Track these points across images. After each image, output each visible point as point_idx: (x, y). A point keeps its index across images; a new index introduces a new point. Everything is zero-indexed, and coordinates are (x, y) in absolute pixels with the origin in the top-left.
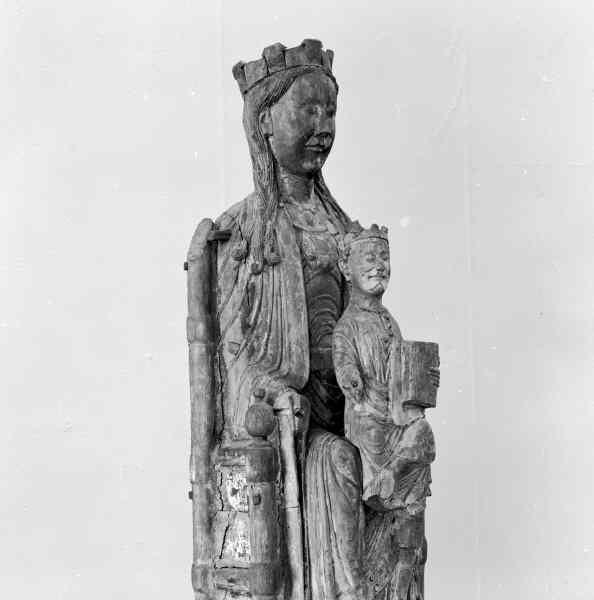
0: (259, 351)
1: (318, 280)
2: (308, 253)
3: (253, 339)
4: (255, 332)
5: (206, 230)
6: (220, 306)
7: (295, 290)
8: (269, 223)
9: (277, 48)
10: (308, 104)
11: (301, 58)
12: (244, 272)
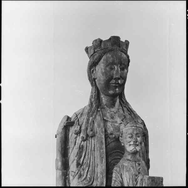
0: (84, 176)
1: (113, 144)
2: (109, 132)
3: (81, 170)
4: (82, 167)
5: (65, 120)
6: (69, 154)
7: (101, 148)
8: (91, 118)
10: (110, 65)
11: (108, 44)
12: (79, 140)
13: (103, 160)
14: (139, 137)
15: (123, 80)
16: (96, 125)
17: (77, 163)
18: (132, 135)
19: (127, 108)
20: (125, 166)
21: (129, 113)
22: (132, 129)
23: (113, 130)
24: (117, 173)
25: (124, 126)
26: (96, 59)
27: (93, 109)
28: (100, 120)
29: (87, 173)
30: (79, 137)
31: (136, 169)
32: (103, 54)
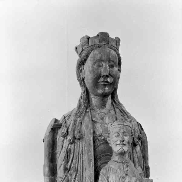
2: (98, 133)
3: (69, 175)
4: (70, 172)
5: (53, 123)
6: (57, 159)
7: (89, 151)
9: (85, 38)
11: (96, 41)
12: (66, 143)
13: (91, 163)
14: (126, 136)
15: (113, 79)
16: (84, 126)
17: (64, 167)
18: (118, 133)
19: (119, 109)
20: (112, 167)
21: (122, 114)
22: (118, 127)
23: (103, 131)
24: (103, 175)
25: (111, 125)
26: (83, 57)
27: (81, 110)
28: (88, 121)
29: (75, 178)
30: (66, 140)
31: (123, 171)
32: (90, 51)
